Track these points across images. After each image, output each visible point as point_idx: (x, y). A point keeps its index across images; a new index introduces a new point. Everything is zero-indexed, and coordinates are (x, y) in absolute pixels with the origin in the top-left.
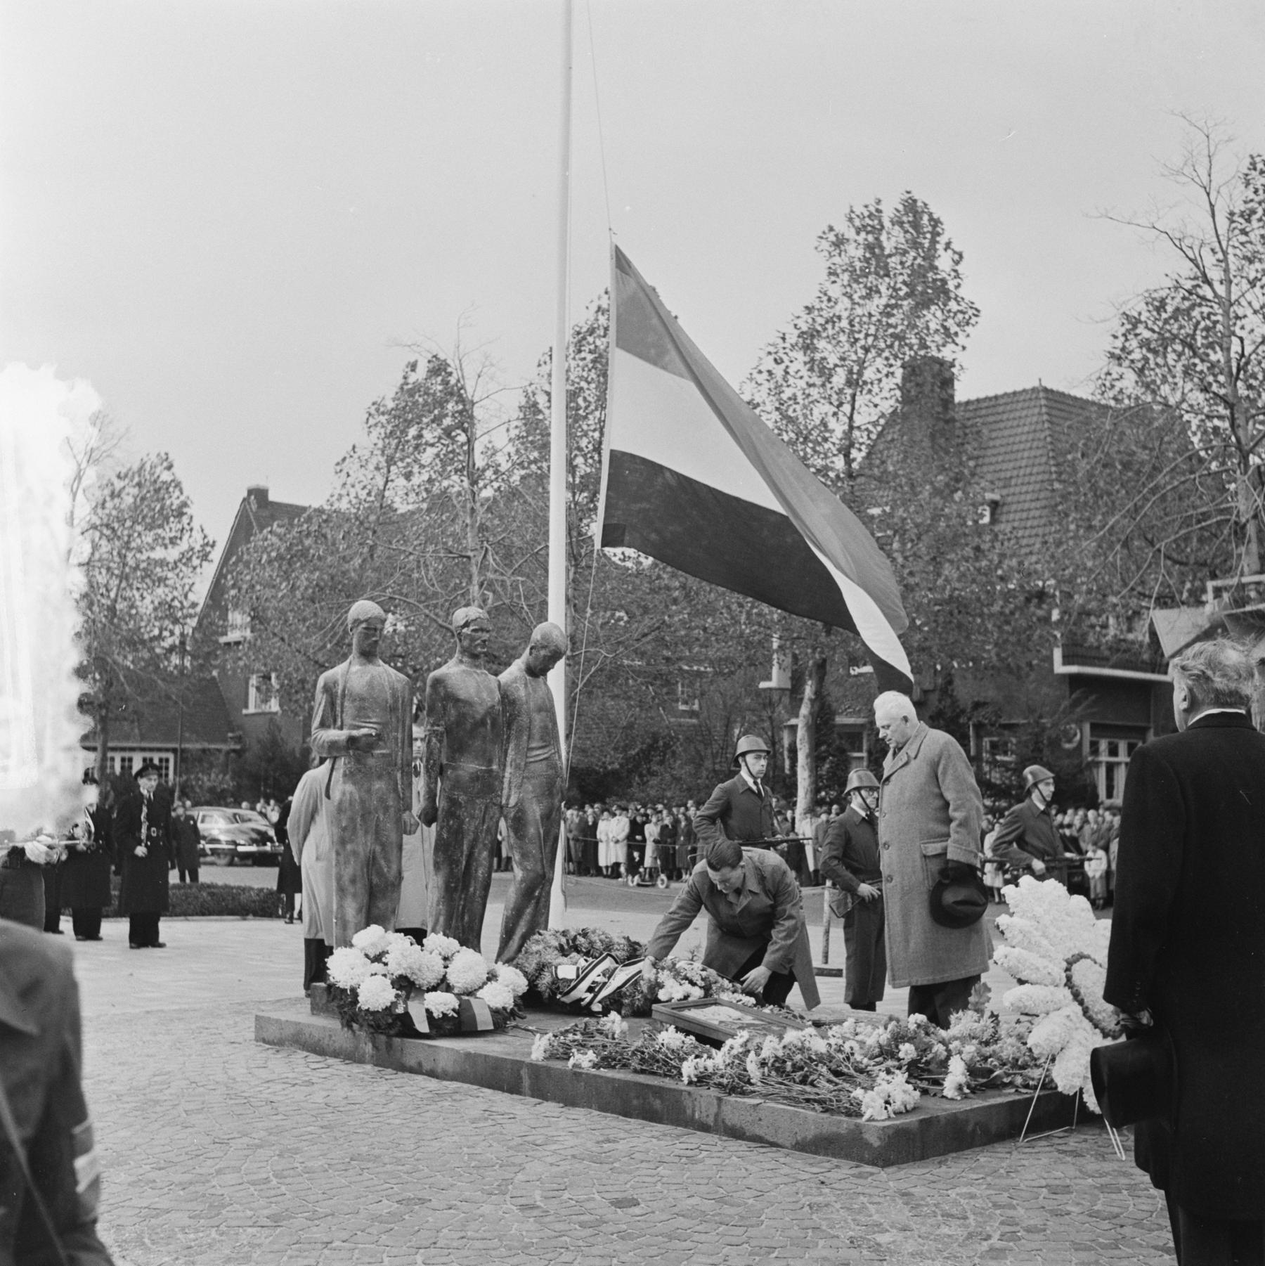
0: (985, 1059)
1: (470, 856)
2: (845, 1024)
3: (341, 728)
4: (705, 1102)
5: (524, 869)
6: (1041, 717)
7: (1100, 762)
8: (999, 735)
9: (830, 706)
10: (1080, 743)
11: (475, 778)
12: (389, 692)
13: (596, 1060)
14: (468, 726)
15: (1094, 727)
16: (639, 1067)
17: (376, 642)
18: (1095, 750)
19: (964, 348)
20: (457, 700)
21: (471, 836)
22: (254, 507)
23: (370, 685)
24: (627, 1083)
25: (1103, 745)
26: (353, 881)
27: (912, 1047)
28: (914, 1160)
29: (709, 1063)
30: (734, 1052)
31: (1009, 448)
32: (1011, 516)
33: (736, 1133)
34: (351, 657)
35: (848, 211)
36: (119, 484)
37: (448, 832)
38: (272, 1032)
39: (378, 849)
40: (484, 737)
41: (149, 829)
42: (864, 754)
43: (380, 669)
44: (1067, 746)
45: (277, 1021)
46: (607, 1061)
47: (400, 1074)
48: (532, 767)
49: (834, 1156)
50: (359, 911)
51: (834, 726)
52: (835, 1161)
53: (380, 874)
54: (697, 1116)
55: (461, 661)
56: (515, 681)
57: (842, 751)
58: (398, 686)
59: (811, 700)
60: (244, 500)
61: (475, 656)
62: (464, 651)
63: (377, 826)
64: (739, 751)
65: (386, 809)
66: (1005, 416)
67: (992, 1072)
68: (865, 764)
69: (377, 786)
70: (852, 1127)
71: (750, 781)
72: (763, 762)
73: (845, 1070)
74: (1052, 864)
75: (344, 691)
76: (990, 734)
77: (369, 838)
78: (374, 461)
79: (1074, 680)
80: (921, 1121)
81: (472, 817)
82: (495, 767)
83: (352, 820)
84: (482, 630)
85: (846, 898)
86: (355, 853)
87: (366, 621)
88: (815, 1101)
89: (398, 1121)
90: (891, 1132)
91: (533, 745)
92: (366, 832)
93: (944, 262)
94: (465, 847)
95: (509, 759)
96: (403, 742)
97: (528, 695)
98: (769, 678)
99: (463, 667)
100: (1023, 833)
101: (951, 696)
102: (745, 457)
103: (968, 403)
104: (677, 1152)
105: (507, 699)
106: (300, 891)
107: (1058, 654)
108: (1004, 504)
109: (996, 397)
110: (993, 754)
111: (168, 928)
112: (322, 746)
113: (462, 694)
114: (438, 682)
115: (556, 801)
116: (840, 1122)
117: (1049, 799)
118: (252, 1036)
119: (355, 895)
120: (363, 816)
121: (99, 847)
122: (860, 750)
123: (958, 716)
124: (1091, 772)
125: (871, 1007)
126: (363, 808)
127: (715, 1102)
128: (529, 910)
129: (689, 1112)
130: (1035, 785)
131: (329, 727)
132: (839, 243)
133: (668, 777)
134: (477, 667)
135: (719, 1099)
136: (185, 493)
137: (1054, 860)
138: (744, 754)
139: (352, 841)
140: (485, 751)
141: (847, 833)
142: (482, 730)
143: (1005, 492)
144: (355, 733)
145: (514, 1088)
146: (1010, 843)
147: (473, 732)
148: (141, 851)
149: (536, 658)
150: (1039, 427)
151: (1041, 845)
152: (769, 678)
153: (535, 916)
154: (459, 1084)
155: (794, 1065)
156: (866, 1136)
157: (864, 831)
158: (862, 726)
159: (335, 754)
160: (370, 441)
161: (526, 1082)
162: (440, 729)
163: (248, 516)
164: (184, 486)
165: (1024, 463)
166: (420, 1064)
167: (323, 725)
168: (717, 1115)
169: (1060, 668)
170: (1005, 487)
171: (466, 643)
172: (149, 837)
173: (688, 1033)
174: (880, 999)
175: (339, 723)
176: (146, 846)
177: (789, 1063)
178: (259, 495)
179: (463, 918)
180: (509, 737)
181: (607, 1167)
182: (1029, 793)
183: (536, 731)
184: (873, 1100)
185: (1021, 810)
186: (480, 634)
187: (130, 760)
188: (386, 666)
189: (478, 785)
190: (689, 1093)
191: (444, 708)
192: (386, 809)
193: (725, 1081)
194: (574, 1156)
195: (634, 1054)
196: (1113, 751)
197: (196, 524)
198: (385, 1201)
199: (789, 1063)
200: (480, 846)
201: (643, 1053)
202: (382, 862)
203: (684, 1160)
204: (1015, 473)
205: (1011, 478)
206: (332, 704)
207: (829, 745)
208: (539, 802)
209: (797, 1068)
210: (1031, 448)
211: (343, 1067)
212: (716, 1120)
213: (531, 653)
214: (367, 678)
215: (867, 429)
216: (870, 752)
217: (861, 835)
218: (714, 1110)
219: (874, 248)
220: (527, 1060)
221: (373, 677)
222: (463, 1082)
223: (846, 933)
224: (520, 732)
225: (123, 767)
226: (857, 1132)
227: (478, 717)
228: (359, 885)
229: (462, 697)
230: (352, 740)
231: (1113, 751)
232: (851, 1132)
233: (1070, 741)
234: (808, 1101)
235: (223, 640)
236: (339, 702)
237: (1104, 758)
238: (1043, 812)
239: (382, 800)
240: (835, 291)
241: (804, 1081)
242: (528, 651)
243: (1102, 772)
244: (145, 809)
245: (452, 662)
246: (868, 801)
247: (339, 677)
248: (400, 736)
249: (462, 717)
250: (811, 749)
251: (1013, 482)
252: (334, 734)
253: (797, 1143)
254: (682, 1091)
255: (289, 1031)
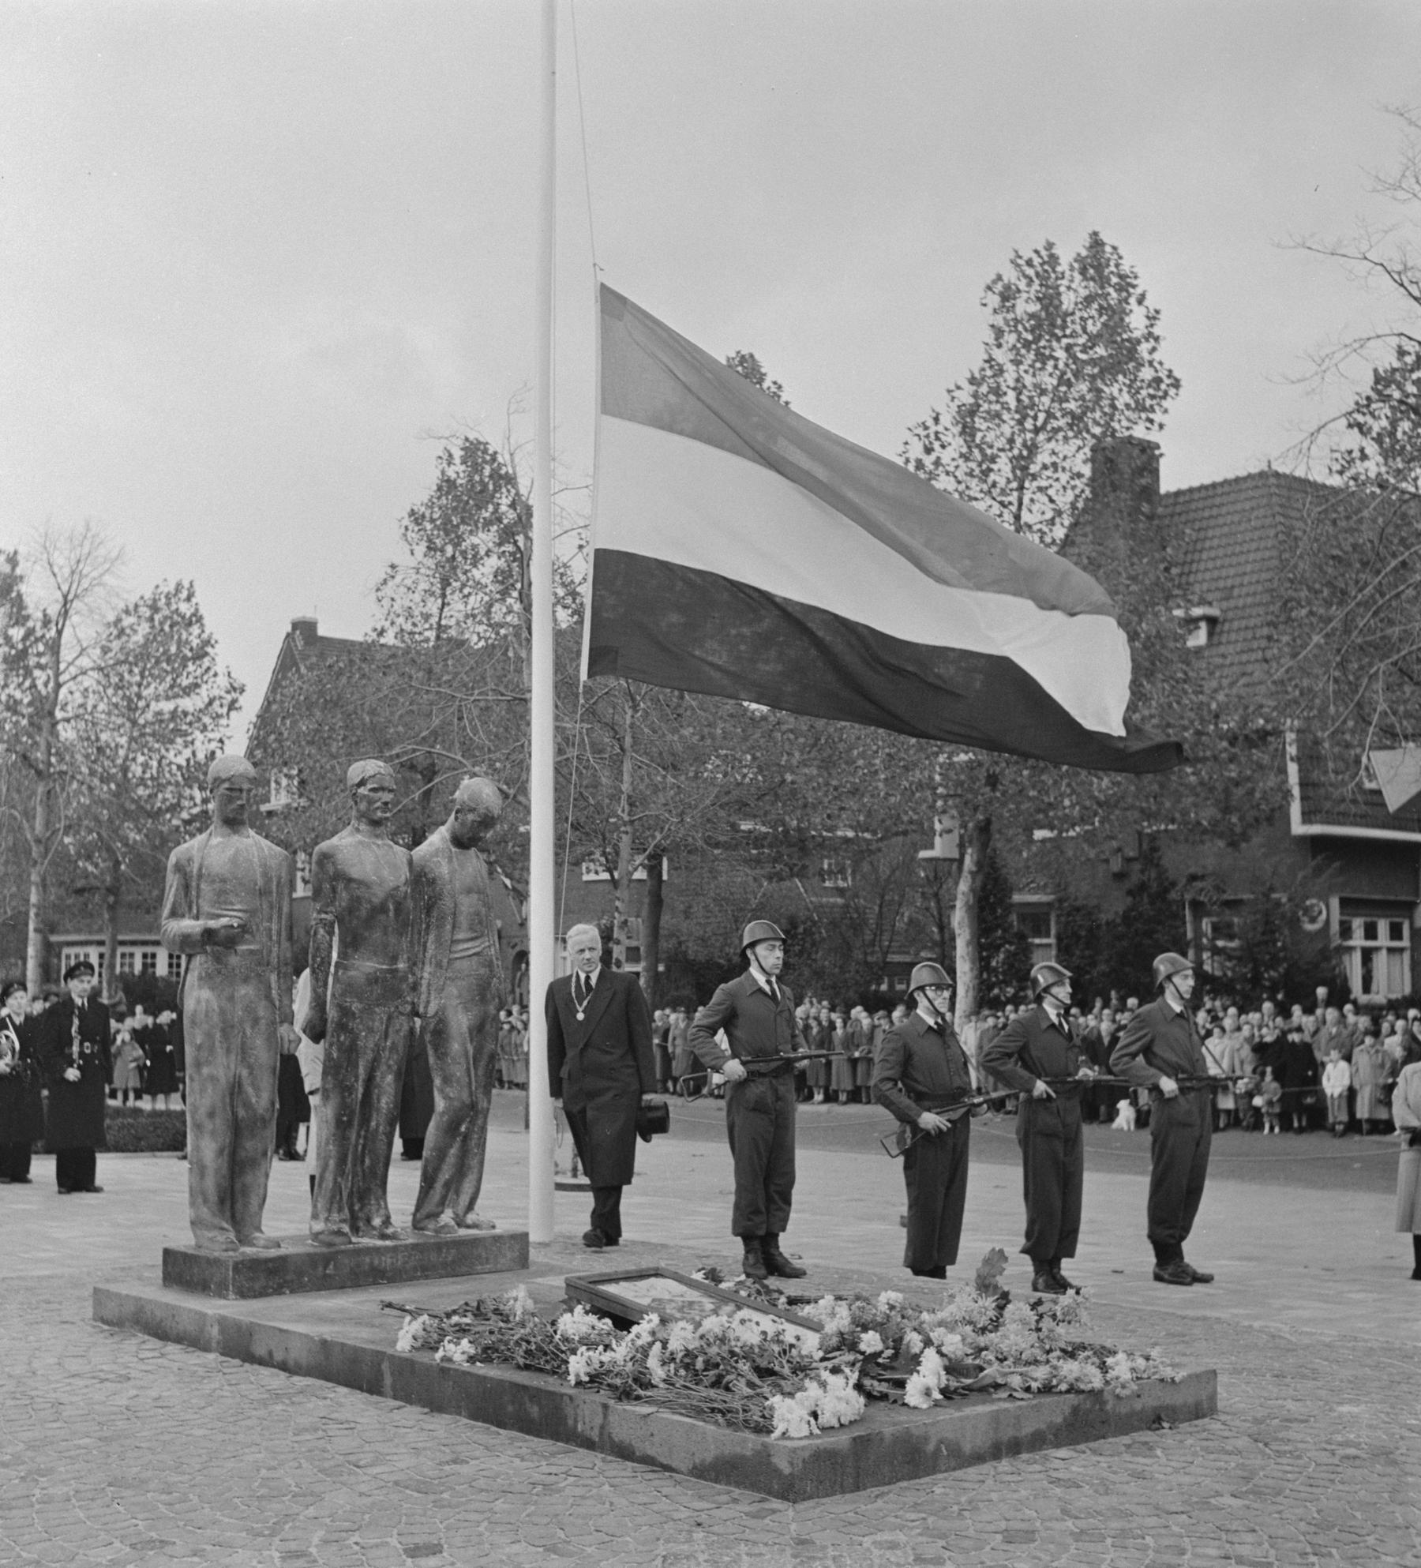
0: (979, 1350)
1: (370, 1080)
2: (821, 1302)
3: (197, 918)
4: (588, 1410)
5: (446, 1097)
6: (1272, 889)
7: (1351, 949)
8: (1218, 915)
9: (1006, 880)
10: (1327, 922)
11: (373, 980)
12: (259, 870)
13: (472, 1351)
14: (363, 913)
15: (1345, 903)
16: (521, 1361)
17: (242, 806)
18: (1346, 931)
19: (1161, 426)
20: (350, 880)
21: (370, 1055)
22: (300, 644)
23: (234, 860)
24: (501, 1382)
25: (1358, 924)
26: (211, 1115)
27: (878, 1336)
28: (843, 1492)
29: (607, 1357)
30: (639, 1343)
31: (1229, 551)
32: (1233, 636)
33: (624, 1453)
34: (212, 827)
35: (1012, 255)
36: (127, 621)
37: (339, 1050)
38: (111, 1310)
39: (245, 1073)
40: (386, 927)
41: (81, 1044)
42: (1052, 940)
43: (250, 841)
44: (1309, 927)
45: (118, 1295)
46: (487, 1354)
47: (247, 1365)
48: (457, 964)
49: (738, 1485)
50: (220, 1152)
51: (1012, 905)
52: (737, 1492)
53: (247, 1105)
54: (580, 1427)
55: (358, 830)
56: (436, 853)
57: (1022, 937)
58: (273, 863)
59: (971, 872)
60: (288, 635)
61: (376, 823)
62: (362, 816)
63: (243, 1043)
64: (746, 942)
65: (256, 1021)
66: (1224, 510)
67: (982, 1369)
68: (1054, 952)
69: (243, 992)
70: (759, 1447)
71: (761, 980)
72: (779, 954)
73: (777, 1368)
74: (1188, 1084)
75: (200, 869)
76: (1208, 914)
77: (233, 1057)
78: (424, 585)
79: (1317, 844)
80: (854, 1439)
81: (370, 1030)
82: (401, 966)
83: (209, 1035)
84: (382, 789)
85: (904, 1132)
86: (213, 1079)
87: (229, 779)
88: (720, 1411)
89: (201, 1432)
90: (807, 1454)
91: (460, 936)
92: (228, 1051)
93: (1136, 321)
94: (361, 1070)
95: (428, 955)
96: (279, 934)
97: (452, 872)
98: (932, 846)
99: (359, 837)
100: (1152, 1041)
101: (1158, 865)
102: (686, 564)
103: (1178, 493)
104: (537, 1477)
105: (421, 878)
106: (307, 1119)
107: (1295, 809)
108: (1225, 621)
109: (1214, 485)
110: (1214, 939)
111: (106, 1165)
112: (174, 940)
113: (355, 873)
114: (325, 857)
115: (492, 1009)
116: (745, 1440)
117: (1187, 996)
118: (89, 1312)
119: (213, 1133)
120: (223, 1031)
121: (26, 1067)
122: (1048, 935)
123: (1166, 891)
124: (1341, 962)
125: (939, 1272)
126: (224, 1022)
127: (600, 1409)
128: (453, 1151)
129: (570, 1422)
130: (1169, 978)
131: (183, 916)
132: (1008, 295)
133: (807, 972)
134: (377, 836)
135: (605, 1407)
136: (207, 632)
137: (1189, 1079)
138: (752, 945)
139: (208, 1063)
140: (386, 946)
141: (905, 1047)
142: (382, 917)
143: (1225, 604)
144: (213, 924)
145: (373, 1387)
146: (1134, 1056)
147: (369, 921)
148: (72, 1074)
149: (463, 824)
150: (1268, 521)
151: (1174, 1058)
152: (932, 846)
153: (464, 1153)
154: (309, 1381)
155: (707, 1362)
156: (775, 1460)
157: (931, 1046)
158: (1049, 904)
159: (188, 951)
160: (412, 557)
161: (388, 1381)
162: (329, 917)
163: (293, 655)
164: (205, 621)
165: (1249, 568)
166: (270, 1353)
167: (174, 914)
168: (602, 1427)
169: (1298, 828)
170: (1227, 599)
171: (363, 806)
172: (82, 1054)
173: (602, 1313)
174: (953, 1262)
175: (195, 911)
176: (79, 1068)
177: (700, 1359)
178: (305, 629)
179: (363, 1162)
180: (428, 927)
181: (432, 1497)
182: (1161, 990)
183: (463, 920)
184: (790, 1411)
185: (1149, 1012)
186: (380, 794)
187: (154, 956)
188: (257, 837)
189: (378, 990)
190: (571, 1398)
191: (334, 890)
192: (256, 1021)
193: (618, 1381)
194: (396, 1483)
195: (517, 1343)
196: (1371, 932)
197: (220, 668)
198: (117, 1544)
199: (700, 1359)
200: (384, 1068)
201: (528, 1342)
202: (250, 1090)
203: (539, 1488)
204: (1238, 581)
205: (1233, 587)
206: (187, 887)
207: (1005, 931)
208: (467, 1009)
209: (710, 1365)
210: (1258, 549)
211: (184, 1357)
212: (601, 1434)
213: (456, 819)
214: (230, 852)
215: (1040, 530)
216: (1059, 938)
217: (928, 1049)
218: (599, 1420)
219: (1049, 300)
220: (390, 1351)
221: (237, 851)
222: (318, 1377)
223: (907, 1177)
224: (442, 918)
225: (145, 965)
226: (764, 1456)
227: (376, 901)
228: (218, 1121)
229: (355, 876)
230: (209, 934)
231: (1371, 932)
232: (758, 1453)
233: (1313, 920)
234: (713, 1410)
235: (264, 808)
236: (194, 884)
237: (1358, 940)
238: (1180, 1015)
239: (249, 1010)
240: (1002, 356)
241: (716, 1384)
242: (453, 816)
243: (1357, 958)
244: (76, 1021)
245: (344, 833)
246: (936, 1003)
247: (194, 852)
248: (274, 927)
249: (356, 901)
250: (973, 935)
251: (1236, 592)
252: (189, 925)
253: (695, 1467)
254: (562, 1395)
255: (129, 1308)
